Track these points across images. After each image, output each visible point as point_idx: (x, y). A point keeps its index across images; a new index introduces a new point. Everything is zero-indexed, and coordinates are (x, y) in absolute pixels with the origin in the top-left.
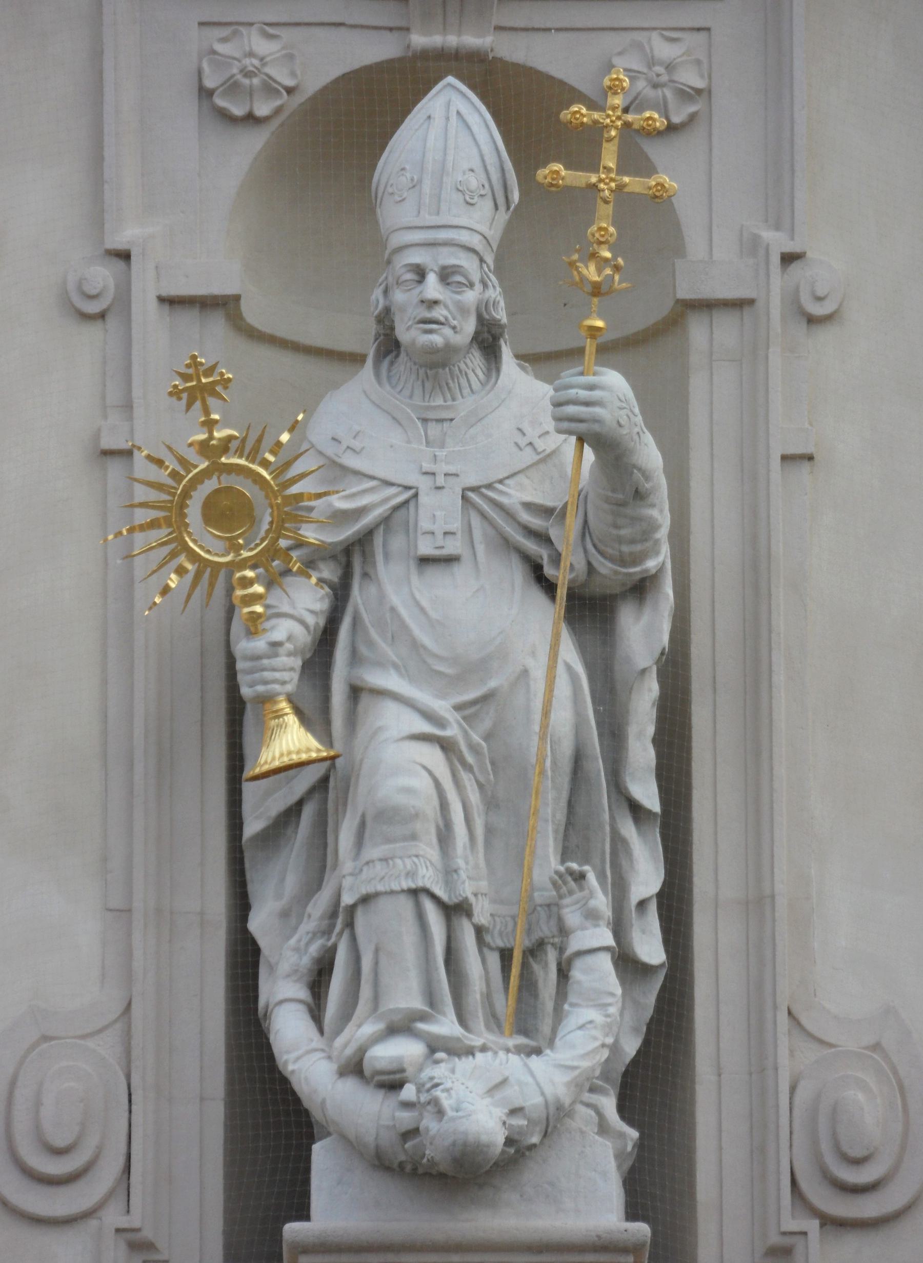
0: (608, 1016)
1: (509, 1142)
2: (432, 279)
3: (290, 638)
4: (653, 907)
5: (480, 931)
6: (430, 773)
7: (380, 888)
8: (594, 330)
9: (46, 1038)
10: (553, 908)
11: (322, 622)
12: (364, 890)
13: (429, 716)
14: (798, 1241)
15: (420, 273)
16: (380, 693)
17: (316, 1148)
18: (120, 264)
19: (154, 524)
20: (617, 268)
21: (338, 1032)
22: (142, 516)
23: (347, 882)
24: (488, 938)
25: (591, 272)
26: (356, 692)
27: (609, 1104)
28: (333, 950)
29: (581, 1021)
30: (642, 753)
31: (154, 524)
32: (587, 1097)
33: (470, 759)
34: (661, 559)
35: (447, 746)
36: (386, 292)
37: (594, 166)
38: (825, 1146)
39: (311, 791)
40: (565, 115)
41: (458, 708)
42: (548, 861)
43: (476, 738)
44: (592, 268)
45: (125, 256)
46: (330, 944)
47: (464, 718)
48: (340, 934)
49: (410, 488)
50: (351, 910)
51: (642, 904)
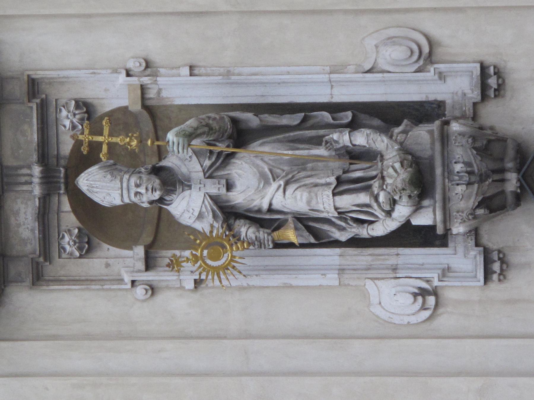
0: (370, 134)
1: (411, 166)
2: (139, 190)
3: (254, 233)
4: (335, 115)
5: (344, 172)
6: (294, 191)
7: (332, 205)
8: (153, 143)
9: (380, 303)
10: (336, 150)
11: (248, 221)
12: (333, 209)
13: (278, 189)
14: (437, 71)
15: (137, 194)
16: (270, 204)
17: (413, 223)
18: (136, 283)
19: (219, 277)
20: (132, 136)
21: (376, 217)
22: (217, 282)
23: (330, 215)
24: (346, 169)
25: (134, 143)
26: (270, 210)
27: (397, 130)
28: (351, 217)
29: (372, 142)
30: (286, 120)
31: (219, 277)
32: (394, 138)
33: (290, 176)
34: (225, 117)
35: (287, 183)
36: (143, 203)
37: (100, 144)
38: (408, 63)
39: (301, 222)
40: (85, 153)
41: (274, 180)
42: (321, 151)
43: (284, 174)
44: (132, 143)
45: (133, 282)
46: (349, 218)
47: (277, 178)
48: (346, 216)
49: (205, 195)
50: (339, 213)
51: (334, 119)
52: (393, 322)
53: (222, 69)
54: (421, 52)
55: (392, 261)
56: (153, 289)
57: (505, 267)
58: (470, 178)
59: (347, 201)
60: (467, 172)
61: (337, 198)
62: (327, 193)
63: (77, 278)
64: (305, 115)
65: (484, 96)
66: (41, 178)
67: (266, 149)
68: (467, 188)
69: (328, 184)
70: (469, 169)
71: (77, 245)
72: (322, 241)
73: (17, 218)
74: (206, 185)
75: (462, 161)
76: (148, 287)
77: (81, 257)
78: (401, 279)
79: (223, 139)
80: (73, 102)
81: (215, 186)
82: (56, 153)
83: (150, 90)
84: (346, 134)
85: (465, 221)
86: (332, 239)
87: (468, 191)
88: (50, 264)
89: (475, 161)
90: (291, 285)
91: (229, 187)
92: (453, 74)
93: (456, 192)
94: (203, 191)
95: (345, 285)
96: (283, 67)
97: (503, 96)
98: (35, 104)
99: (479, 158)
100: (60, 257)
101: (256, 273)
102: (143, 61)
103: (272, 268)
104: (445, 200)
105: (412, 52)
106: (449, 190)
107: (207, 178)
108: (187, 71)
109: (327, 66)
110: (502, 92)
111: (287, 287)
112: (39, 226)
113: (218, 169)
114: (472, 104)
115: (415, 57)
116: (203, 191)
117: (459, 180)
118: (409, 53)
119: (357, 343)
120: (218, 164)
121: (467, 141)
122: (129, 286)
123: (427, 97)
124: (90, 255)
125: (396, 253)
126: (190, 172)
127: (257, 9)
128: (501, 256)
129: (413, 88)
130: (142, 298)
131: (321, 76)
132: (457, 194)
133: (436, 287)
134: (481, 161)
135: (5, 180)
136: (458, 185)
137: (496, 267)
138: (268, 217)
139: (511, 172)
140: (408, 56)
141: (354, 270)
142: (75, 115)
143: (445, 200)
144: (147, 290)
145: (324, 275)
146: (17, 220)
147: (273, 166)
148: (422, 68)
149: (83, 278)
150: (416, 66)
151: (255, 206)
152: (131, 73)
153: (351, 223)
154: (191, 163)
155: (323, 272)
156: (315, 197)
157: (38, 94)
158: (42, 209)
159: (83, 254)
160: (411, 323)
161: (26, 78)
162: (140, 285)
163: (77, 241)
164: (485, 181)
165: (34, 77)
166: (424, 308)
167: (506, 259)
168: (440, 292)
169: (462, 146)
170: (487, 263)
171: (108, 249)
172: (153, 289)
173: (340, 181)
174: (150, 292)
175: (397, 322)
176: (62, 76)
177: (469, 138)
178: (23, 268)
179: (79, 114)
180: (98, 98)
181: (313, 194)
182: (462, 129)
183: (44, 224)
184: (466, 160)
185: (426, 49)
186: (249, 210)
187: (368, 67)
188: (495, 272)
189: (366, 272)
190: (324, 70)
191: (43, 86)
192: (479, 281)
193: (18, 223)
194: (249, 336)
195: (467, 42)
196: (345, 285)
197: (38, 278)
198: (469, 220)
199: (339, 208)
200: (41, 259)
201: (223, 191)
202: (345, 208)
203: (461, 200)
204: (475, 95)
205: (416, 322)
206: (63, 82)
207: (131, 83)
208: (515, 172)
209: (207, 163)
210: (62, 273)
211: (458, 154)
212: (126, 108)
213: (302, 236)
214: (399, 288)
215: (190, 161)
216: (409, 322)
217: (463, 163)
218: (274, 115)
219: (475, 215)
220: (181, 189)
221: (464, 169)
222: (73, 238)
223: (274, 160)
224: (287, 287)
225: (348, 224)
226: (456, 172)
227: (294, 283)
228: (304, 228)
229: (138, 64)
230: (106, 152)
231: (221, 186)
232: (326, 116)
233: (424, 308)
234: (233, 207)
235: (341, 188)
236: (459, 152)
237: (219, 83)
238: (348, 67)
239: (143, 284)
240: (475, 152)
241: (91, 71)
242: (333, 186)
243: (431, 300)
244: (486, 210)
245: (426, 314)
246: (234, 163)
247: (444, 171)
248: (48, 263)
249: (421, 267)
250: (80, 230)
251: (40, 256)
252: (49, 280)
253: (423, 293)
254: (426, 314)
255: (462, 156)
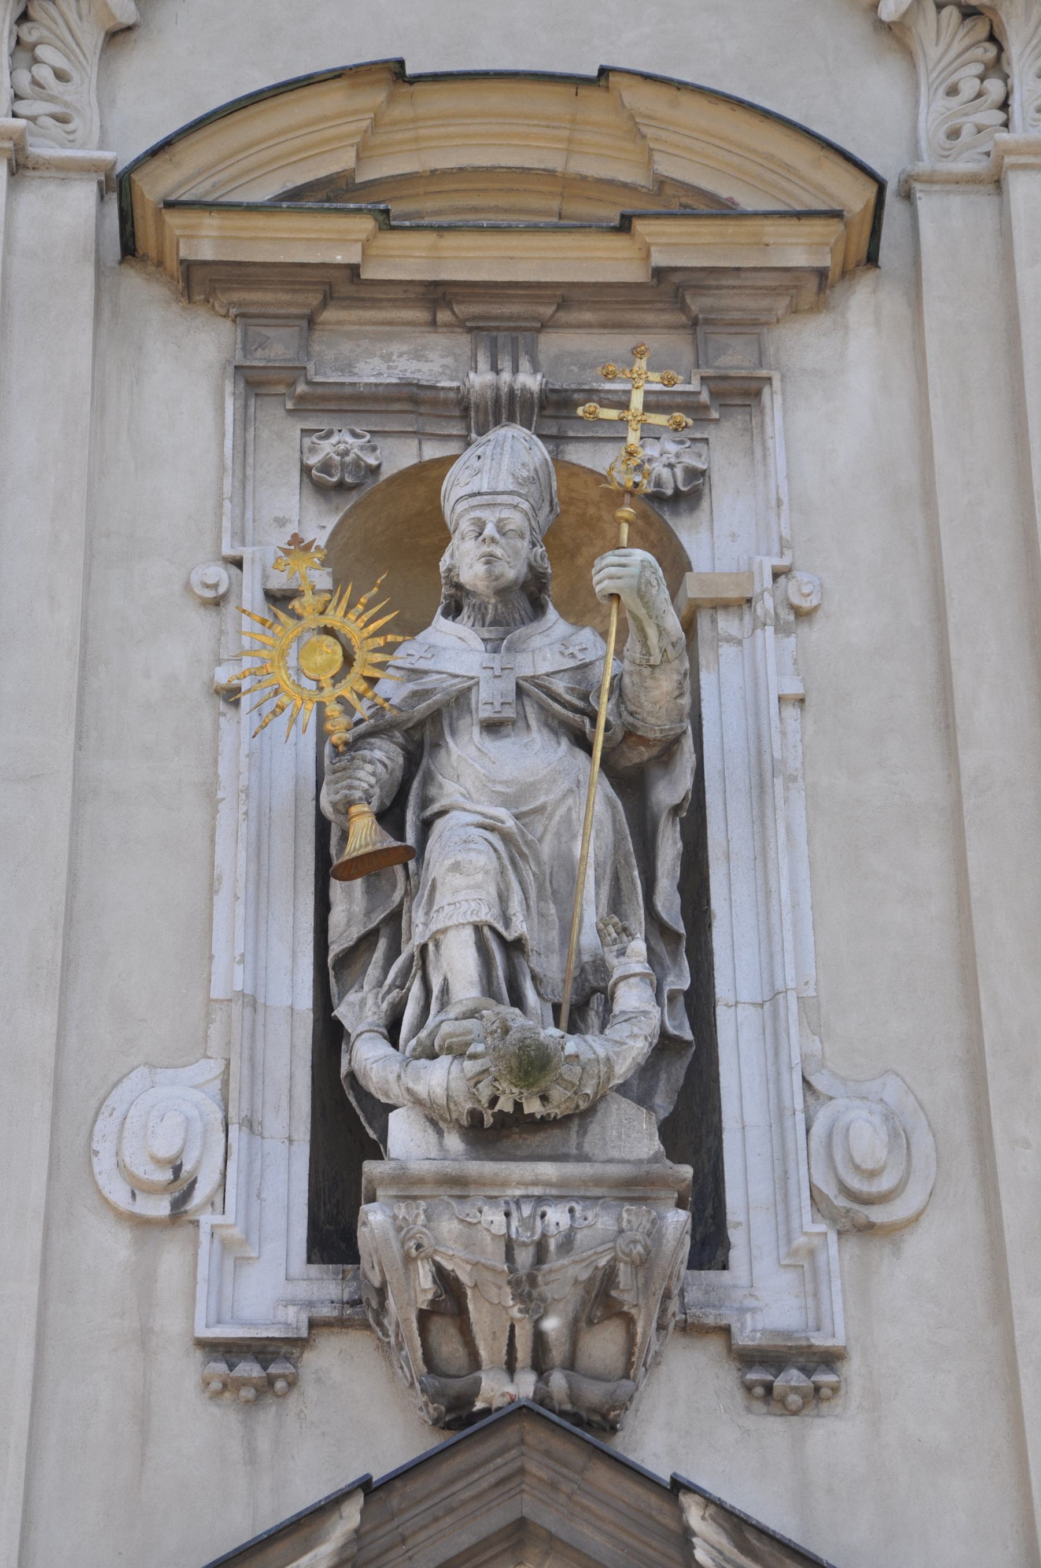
18: (234, 570)
35: (506, 838)
39: (386, 921)
45: (238, 563)
49: (472, 678)
52: (101, 1117)
53: (799, 765)
54: (868, 1201)
55: (275, 1124)
56: (217, 603)
57: (248, 1393)
58: (524, 1244)
59: (459, 965)
60: (544, 1236)
61: (468, 935)
62: (484, 909)
63: (250, 460)
64: (679, 936)
65: (747, 1358)
66: (512, 392)
67: (599, 808)
68: (495, 1237)
69: (507, 922)
70: (552, 1244)
71: (338, 458)
72: (332, 972)
73: (405, 357)
74: (497, 681)
75: (576, 1225)
76: (222, 590)
77: (305, 470)
78: (223, 1135)
79: (625, 714)
80: (705, 467)
81: (499, 697)
82: (571, 434)
83: (737, 622)
84: (645, 968)
85: (399, 1229)
86: (335, 1000)
87: (489, 1238)
88: (289, 411)
89: (575, 1262)
90: (217, 892)
91: (493, 727)
92: (809, 1287)
93: (485, 1209)
94: (483, 675)
95: (208, 1014)
96: (809, 894)
97: (748, 1410)
98: (698, 389)
99: (584, 1276)
100: (305, 432)
101: (253, 814)
102: (815, 603)
103: (265, 847)
104: (458, 1185)
105: (872, 1175)
106: (492, 1197)
107: (517, 684)
108: (793, 687)
109: (816, 990)
110: (759, 1406)
111: (211, 885)
112: (388, 385)
113: (542, 708)
114: (724, 1322)
115: (855, 1183)
116: (483, 675)
117: (521, 1220)
118: (868, 1165)
119: (49, 1021)
120: (557, 707)
121: (635, 1242)
122: (227, 551)
123: (738, 1224)
124: (308, 490)
125: (295, 1137)
126: (533, 651)
127: (970, 833)
128: (280, 1385)
129: (762, 1190)
130: (195, 579)
131: (790, 973)
132: (481, 1212)
133: (196, 1224)
134: (576, 1282)
135: (502, 336)
136: (507, 1215)
137: (249, 1369)
138: (410, 817)
139: (537, 1382)
140: (858, 1161)
141: (253, 1035)
142: (671, 466)
143: (458, 1185)
144: (215, 586)
145: (242, 961)
146: (401, 355)
147: (550, 818)
148: (823, 1206)
149: (249, 472)
150: (829, 1189)
151: (441, 787)
152: (782, 580)
153: (390, 998)
154: (558, 656)
155: (249, 958)
156: (472, 882)
157: (721, 405)
158: (430, 394)
159: (313, 471)
160: (95, 1160)
161: (763, 373)
162: (230, 578)
163: (348, 459)
164: (517, 1297)
165: (766, 391)
166: (138, 1188)
167: (269, 1400)
168: (182, 1233)
169: (621, 1231)
170: (262, 1351)
171: (324, 527)
172: (217, 603)
173: (514, 948)
174: (209, 594)
175: (99, 1126)
176: (770, 443)
177: (645, 1247)
178: (278, 348)
179: (674, 476)
180: (712, 520)
181: (480, 877)
182: (671, 1229)
183: (389, 399)
184: (579, 1236)
185: (877, 1215)
186: (429, 779)
187: (819, 1082)
188: (231, 1367)
189: (246, 1056)
190: (806, 983)
191: (739, 418)
192: (207, 1326)
193: (394, 357)
194: (79, 799)
195: (900, 1321)
196: (208, 1014)
197: (253, 382)
198: (403, 1243)
199: (437, 946)
200: (301, 388)
201: (485, 713)
202: (438, 960)
203: (462, 1221)
204: (749, 1333)
205: (97, 1169)
206: (753, 453)
207: (757, 578)
208: (535, 1393)
209: (560, 686)
210: (265, 434)
211: (597, 1215)
212: (691, 569)
213: (349, 924)
214: (198, 1127)
215: (562, 654)
216: (96, 1153)
217: (572, 1228)
218: (678, 869)
219: (415, 1259)
220: (486, 636)
221: (552, 1230)
222: (356, 450)
223: (567, 820)
224: (211, 885)
225: (389, 992)
226: (546, 1208)
227: (221, 901)
228: (371, 926)
229: (806, 591)
230: (601, 416)
231: (498, 708)
232: (681, 980)
233: (138, 1188)
234: (437, 745)
235: (494, 946)
236: (600, 1220)
237: (760, 753)
238: (816, 1038)
239: (230, 584)
240: (603, 1262)
241: (785, 499)
242: (501, 929)
243: (161, 1208)
244: (430, 1296)
245: (119, 1194)
246: (559, 743)
247: (548, 1184)
248: (289, 405)
249: (253, 1194)
250: (375, 470)
251: (309, 383)
252: (246, 407)
253: (181, 1190)
254: (119, 1194)
255: (590, 1226)
